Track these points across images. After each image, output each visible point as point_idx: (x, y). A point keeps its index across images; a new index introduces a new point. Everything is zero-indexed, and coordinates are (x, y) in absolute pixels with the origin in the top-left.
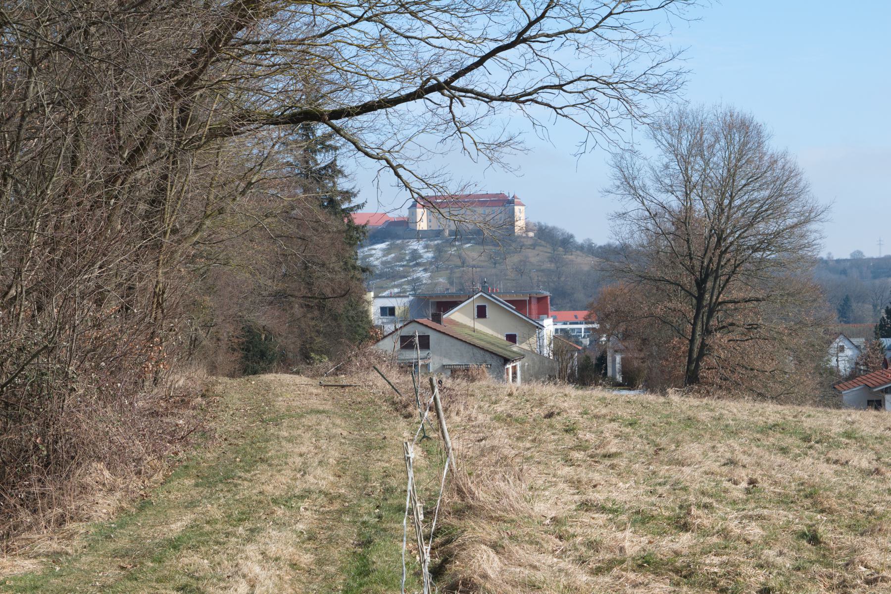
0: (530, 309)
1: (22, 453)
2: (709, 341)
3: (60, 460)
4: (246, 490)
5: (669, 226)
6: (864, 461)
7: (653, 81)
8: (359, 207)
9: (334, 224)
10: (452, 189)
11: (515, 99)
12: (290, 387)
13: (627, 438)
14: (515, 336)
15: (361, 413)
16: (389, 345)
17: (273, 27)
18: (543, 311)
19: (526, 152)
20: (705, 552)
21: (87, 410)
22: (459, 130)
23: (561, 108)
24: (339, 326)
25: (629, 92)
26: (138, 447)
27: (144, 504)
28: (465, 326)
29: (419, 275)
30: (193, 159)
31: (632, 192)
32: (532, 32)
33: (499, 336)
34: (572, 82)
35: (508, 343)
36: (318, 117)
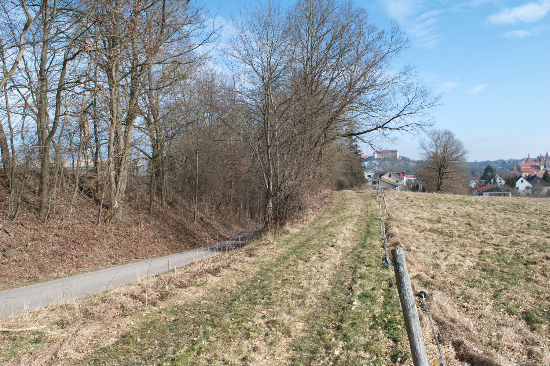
1: (295, 207)
3: (302, 209)
4: (341, 215)
5: (432, 156)
6: (480, 207)
7: (429, 124)
9: (357, 157)
10: (384, 149)
11: (397, 129)
12: (349, 193)
13: (425, 203)
15: (365, 198)
16: (370, 183)
17: (343, 116)
18: (404, 175)
20: (445, 228)
21: (307, 198)
26: (318, 206)
27: (320, 218)
30: (328, 144)
36: (354, 135)
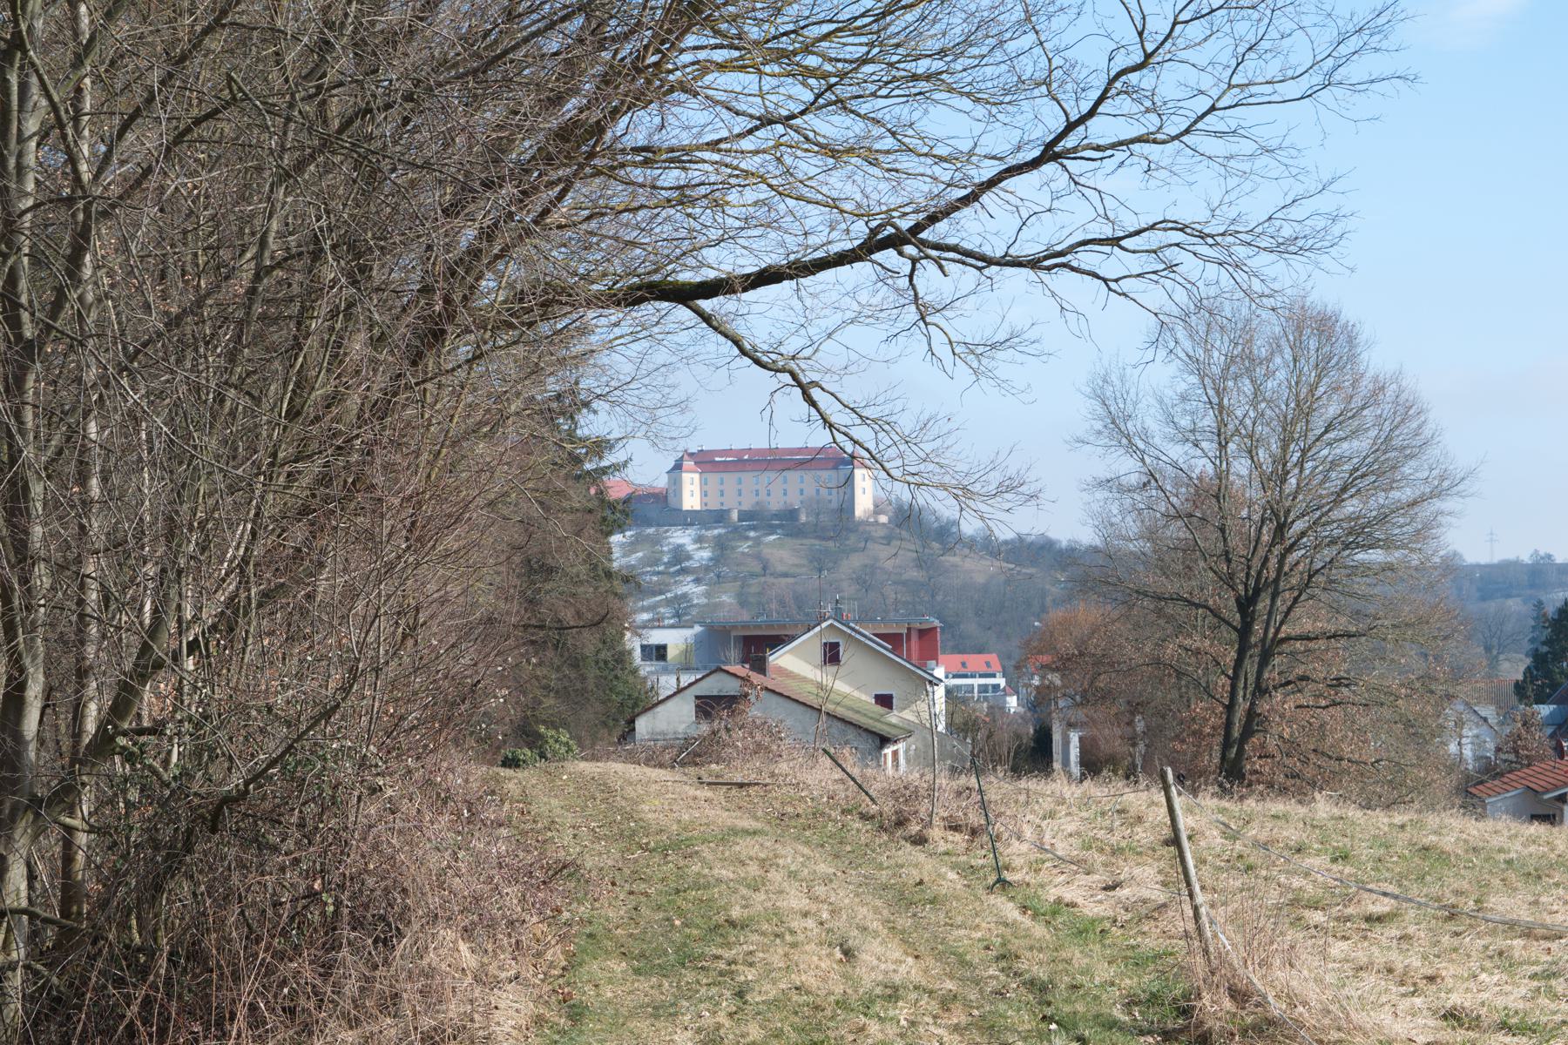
0: (909, 650)
2: (1263, 706)
8: (616, 467)
11: (1034, 264)
14: (891, 697)
19: (1044, 358)
22: (923, 318)
23: (1116, 281)
24: (583, 678)
25: (1241, 252)
28: (804, 680)
29: (685, 589)
31: (1124, 441)
32: (1070, 142)
33: (864, 697)
34: (1138, 233)
35: (880, 709)
